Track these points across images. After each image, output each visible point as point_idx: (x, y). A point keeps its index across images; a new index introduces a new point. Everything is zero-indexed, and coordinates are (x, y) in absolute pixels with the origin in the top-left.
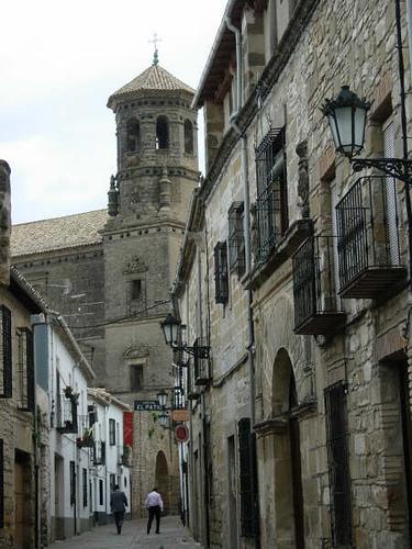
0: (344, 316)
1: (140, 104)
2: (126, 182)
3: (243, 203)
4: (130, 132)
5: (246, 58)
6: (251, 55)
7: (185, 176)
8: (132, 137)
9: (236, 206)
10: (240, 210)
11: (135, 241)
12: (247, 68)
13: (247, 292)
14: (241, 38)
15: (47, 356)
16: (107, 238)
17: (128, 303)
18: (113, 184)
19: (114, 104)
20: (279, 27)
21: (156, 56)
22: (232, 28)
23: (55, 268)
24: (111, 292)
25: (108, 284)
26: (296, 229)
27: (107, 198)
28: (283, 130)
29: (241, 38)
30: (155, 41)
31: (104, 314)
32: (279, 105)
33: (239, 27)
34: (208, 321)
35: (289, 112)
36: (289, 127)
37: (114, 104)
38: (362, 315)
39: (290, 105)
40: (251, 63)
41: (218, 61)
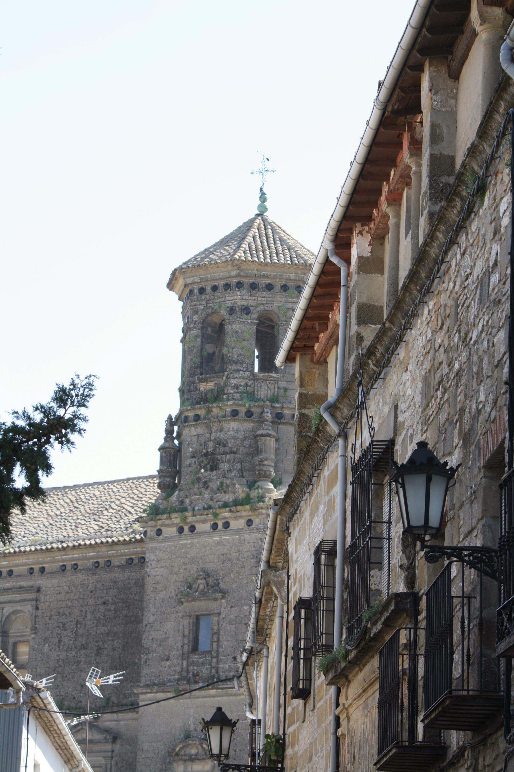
0: (445, 748)
1: (227, 286)
2: (193, 431)
3: (335, 542)
4: (206, 338)
5: (354, 310)
6: (361, 308)
7: (39, 718)
8: (209, 348)
9: (326, 547)
10: (332, 553)
11: (204, 540)
12: (354, 328)
13: (333, 689)
14: (349, 275)
15: (18, 758)
16: (152, 533)
17: (184, 656)
18: (169, 432)
19: (181, 282)
20: (335, 351)
21: (263, 197)
22: (334, 260)
23: (55, 581)
24: (154, 634)
25: (149, 617)
26: (392, 607)
27: (157, 456)
28: (392, 443)
29: (349, 275)
30: (264, 171)
31: (139, 674)
32: (390, 401)
33: (348, 261)
34: (463, 639)
35: (401, 419)
36: (399, 440)
37: (181, 282)
38: (462, 750)
39: (402, 406)
40: (362, 320)
41: (319, 290)
